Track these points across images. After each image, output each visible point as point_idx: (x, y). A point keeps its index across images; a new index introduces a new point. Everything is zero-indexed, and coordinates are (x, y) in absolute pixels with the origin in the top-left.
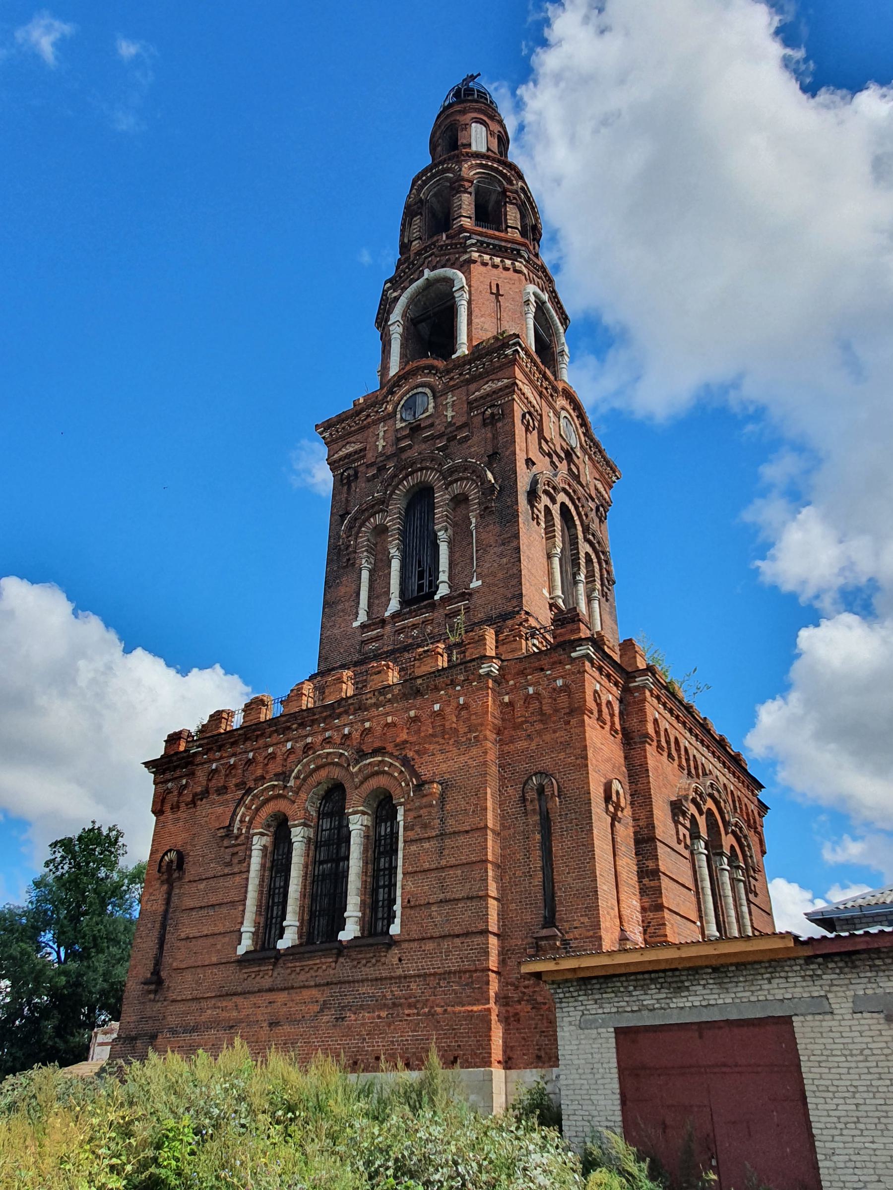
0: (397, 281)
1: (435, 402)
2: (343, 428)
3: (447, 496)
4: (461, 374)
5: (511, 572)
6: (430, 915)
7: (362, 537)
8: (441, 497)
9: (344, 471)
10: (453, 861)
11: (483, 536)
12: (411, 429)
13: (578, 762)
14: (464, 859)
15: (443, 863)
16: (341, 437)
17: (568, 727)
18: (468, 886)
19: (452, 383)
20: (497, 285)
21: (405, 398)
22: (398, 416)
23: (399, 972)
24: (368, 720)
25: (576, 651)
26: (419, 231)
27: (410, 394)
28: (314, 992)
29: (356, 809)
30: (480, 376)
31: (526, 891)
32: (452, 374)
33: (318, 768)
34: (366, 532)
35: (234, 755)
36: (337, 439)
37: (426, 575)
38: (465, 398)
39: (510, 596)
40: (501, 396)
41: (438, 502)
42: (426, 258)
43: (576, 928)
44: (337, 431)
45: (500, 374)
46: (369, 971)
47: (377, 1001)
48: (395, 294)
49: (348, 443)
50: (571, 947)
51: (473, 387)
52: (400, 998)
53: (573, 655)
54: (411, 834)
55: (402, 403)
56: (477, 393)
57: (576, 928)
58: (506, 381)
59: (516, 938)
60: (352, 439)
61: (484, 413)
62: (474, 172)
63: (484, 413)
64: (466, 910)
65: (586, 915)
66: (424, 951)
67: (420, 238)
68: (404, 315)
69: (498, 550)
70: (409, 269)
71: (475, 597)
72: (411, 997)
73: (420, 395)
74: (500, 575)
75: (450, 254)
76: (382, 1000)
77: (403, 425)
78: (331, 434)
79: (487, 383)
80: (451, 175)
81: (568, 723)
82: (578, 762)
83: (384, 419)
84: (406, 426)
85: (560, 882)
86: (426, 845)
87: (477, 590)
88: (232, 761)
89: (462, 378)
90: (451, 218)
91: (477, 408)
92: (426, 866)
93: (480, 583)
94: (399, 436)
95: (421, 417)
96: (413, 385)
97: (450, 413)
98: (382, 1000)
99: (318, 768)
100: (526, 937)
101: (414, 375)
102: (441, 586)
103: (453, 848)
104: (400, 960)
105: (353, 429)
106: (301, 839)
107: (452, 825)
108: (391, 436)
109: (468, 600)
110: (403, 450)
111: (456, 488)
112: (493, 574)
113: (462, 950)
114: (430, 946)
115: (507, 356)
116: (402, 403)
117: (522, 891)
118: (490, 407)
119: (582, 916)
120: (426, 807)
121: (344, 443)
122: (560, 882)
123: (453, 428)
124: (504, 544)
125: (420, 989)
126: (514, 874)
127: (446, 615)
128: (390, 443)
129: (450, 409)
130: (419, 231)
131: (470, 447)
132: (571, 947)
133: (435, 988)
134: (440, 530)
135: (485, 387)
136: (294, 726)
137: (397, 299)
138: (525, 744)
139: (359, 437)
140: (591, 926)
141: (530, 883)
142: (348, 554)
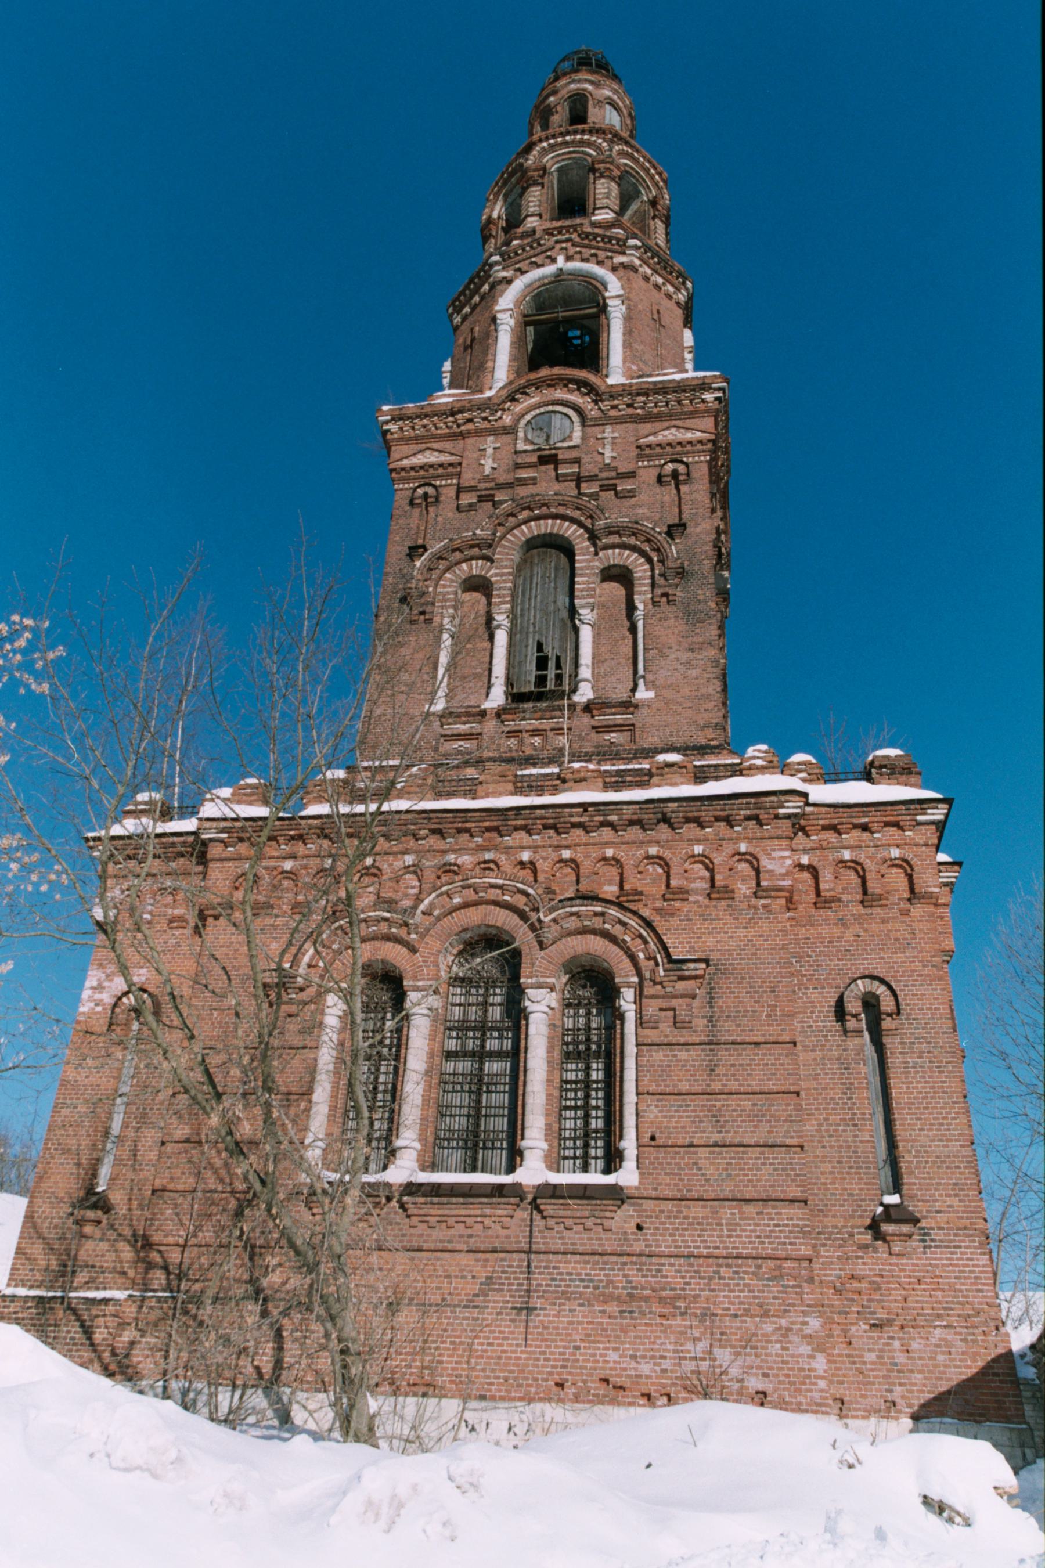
0: (510, 258)
1: (583, 431)
2: (424, 426)
3: (597, 564)
4: (629, 406)
5: (704, 691)
6: (696, 1164)
7: (444, 586)
8: (586, 561)
9: (419, 487)
10: (734, 1086)
11: (658, 631)
12: (540, 457)
13: (926, 971)
14: (754, 1085)
15: (717, 1086)
16: (416, 438)
17: (907, 919)
18: (765, 1128)
19: (613, 413)
20: (658, 312)
21: (533, 413)
22: (521, 434)
23: (638, 1247)
24: (567, 847)
25: (926, 814)
26: (539, 206)
27: (542, 410)
28: (465, 1259)
29: (542, 980)
30: (658, 417)
31: (849, 1147)
32: (616, 402)
33: (465, 905)
34: (452, 581)
35: (294, 857)
36: (410, 438)
37: (551, 664)
38: (632, 439)
39: (702, 723)
40: (688, 452)
41: (581, 568)
42: (557, 242)
43: (938, 1212)
44: (413, 428)
45: (689, 423)
46: (577, 1238)
47: (596, 1288)
48: (504, 274)
49: (428, 449)
50: (932, 1240)
51: (647, 427)
52: (643, 1288)
53: (920, 818)
54: (651, 1035)
55: (528, 417)
56: (651, 438)
57: (938, 1212)
58: (699, 434)
59: (834, 1216)
60: (435, 446)
61: (662, 466)
62: (625, 161)
63: (662, 466)
64: (764, 1164)
65: (956, 1195)
66: (686, 1218)
67: (540, 216)
68: (518, 303)
69: (685, 656)
70: (532, 247)
71: (644, 711)
72: (664, 1289)
73: (559, 416)
74: (686, 691)
75: (598, 248)
76: (606, 1287)
77: (529, 448)
78: (401, 429)
79: (668, 428)
80: (594, 153)
81: (906, 913)
82: (926, 971)
83: (494, 432)
84: (534, 451)
85: (907, 1141)
86: (683, 1055)
87: (648, 704)
88: (288, 865)
89: (630, 411)
90: (524, 214)
91: (649, 457)
92: (684, 1087)
93: (651, 694)
94: (519, 461)
95: (405, 463)
96: (545, 399)
97: (608, 453)
98: (606, 1287)
99: (465, 905)
100: (852, 1217)
101: (550, 386)
102: (582, 685)
103: (733, 1065)
104: (639, 1227)
105: (439, 432)
106: (426, 1012)
107: (728, 1030)
108: (507, 458)
109: (632, 714)
110: (522, 482)
111: (615, 557)
112: (676, 688)
113: (758, 1225)
114: (697, 1210)
115: (704, 401)
116: (528, 417)
117: (841, 1147)
118: (672, 461)
119: (949, 1195)
120: (683, 996)
121: (424, 446)
122: (907, 1141)
123: (492, 485)
124: (692, 650)
125: (683, 1277)
126: (826, 1119)
127: (594, 727)
128: (504, 467)
129: (608, 447)
130: (539, 206)
131: (633, 507)
132: (932, 1240)
133: (711, 1278)
134: (583, 607)
135: (666, 433)
136: (423, 832)
137: (509, 282)
138: (836, 931)
139: (448, 445)
140: (964, 1212)
141: (856, 1136)
142: (423, 605)
